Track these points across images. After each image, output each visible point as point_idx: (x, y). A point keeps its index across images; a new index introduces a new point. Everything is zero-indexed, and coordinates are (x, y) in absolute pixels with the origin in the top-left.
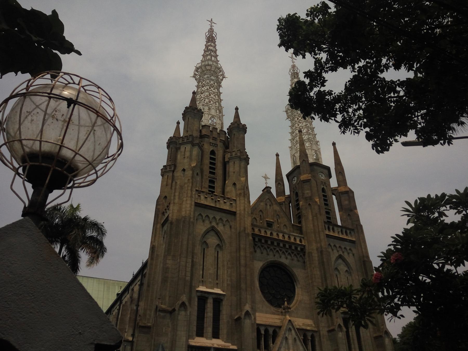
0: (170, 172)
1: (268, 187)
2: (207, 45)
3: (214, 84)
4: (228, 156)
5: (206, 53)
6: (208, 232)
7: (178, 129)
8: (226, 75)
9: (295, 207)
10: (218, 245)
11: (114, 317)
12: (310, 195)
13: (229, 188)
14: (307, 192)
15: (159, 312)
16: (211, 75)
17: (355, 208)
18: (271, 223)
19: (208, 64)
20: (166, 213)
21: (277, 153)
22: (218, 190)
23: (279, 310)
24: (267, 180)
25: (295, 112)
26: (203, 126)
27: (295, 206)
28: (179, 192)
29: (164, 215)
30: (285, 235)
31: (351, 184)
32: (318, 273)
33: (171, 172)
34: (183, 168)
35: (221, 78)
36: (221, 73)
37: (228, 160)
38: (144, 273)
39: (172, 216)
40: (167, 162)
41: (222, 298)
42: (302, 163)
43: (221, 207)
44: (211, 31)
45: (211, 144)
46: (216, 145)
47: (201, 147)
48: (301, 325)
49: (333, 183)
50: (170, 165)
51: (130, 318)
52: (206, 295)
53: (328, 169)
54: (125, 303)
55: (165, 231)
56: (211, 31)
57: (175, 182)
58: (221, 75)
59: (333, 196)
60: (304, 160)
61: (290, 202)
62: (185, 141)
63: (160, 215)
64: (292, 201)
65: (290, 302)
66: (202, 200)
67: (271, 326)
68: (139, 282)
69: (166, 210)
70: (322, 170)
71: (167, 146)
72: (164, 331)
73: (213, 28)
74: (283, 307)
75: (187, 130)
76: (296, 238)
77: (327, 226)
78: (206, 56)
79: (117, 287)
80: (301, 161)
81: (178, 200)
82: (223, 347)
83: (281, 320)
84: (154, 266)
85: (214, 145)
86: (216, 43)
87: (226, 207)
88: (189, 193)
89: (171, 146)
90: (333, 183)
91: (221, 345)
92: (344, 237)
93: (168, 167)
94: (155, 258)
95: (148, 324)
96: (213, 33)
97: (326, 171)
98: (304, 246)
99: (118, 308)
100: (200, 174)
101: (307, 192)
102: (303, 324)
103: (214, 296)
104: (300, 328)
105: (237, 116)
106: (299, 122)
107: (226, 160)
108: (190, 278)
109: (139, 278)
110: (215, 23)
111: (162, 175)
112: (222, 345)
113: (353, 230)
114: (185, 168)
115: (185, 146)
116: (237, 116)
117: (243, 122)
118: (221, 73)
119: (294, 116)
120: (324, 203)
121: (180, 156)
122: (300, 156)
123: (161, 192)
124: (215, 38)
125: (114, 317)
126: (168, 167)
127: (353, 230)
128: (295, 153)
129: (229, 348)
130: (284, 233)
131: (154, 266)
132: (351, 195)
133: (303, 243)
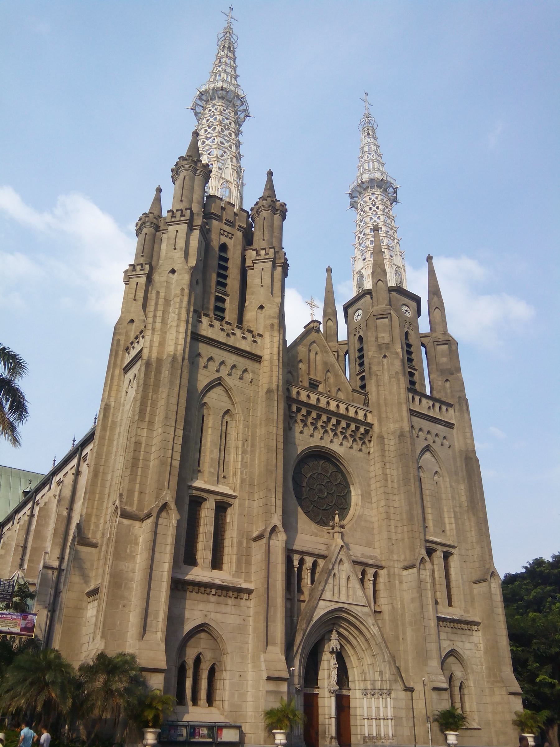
0: (142, 277)
1: (316, 320)
2: (219, 55)
3: (230, 124)
4: (251, 254)
5: (217, 69)
6: (212, 388)
7: (157, 200)
8: (251, 112)
9: (356, 362)
10: (227, 412)
11: (21, 528)
12: (387, 340)
13: (250, 314)
14: (383, 335)
15: (120, 518)
16: (225, 108)
17: (458, 370)
18: (317, 383)
19: (222, 87)
20: (132, 349)
21: (329, 266)
22: (230, 314)
23: (324, 530)
24: (314, 309)
25: (366, 197)
26: (209, 197)
27: (356, 359)
28: (163, 311)
29: (129, 353)
30: (340, 404)
31: (453, 330)
32: (394, 472)
33: (145, 277)
34: (171, 268)
35: (242, 116)
36: (244, 107)
37: (252, 265)
38: (83, 455)
39: (150, 352)
40: (136, 259)
41: (231, 501)
42: (375, 285)
43: (237, 346)
44: (228, 32)
45: (222, 232)
46: (230, 236)
47: (205, 234)
48: (359, 555)
49: (424, 326)
50: (142, 265)
51: (56, 530)
52: (204, 495)
53: (417, 300)
54: (44, 506)
55: (135, 376)
56: (228, 32)
57: (155, 292)
58: (244, 111)
59: (422, 347)
60: (380, 280)
61: (347, 352)
62: (177, 219)
63: (120, 353)
64: (352, 350)
65: (342, 517)
66: (204, 330)
67: (310, 554)
68: (74, 469)
69: (132, 343)
70: (407, 301)
71: (137, 231)
72: (128, 551)
73: (232, 27)
74: (331, 524)
75: (182, 198)
76: (359, 411)
77: (411, 395)
78: (217, 73)
79: (23, 480)
80: (375, 281)
81: (160, 324)
82: (230, 585)
83: (326, 546)
84: (107, 440)
85: (226, 234)
86: (237, 54)
87: (244, 345)
88: (182, 313)
89: (145, 230)
90: (424, 326)
91: (226, 581)
92: (437, 416)
93: (138, 267)
94: (109, 428)
95: (93, 540)
96: (232, 37)
97: (414, 304)
98: (371, 425)
99: (28, 513)
100: (200, 282)
101: (383, 335)
102: (362, 554)
103: (219, 498)
104: (358, 561)
105: (270, 187)
106: (377, 213)
107: (248, 263)
108: (179, 462)
109: (74, 462)
110: (235, 20)
111: (126, 282)
112: (228, 581)
113: (450, 405)
114: (175, 269)
115: (178, 227)
116: (270, 187)
117: (281, 197)
118: (244, 107)
119: (363, 204)
120: (407, 357)
121: (167, 246)
122: (373, 273)
123: (122, 313)
124: (235, 45)
125: (22, 529)
126: (138, 267)
127: (450, 405)
128: (363, 268)
129: (239, 586)
130: (339, 401)
131: (107, 440)
132: (453, 347)
133: (369, 420)
